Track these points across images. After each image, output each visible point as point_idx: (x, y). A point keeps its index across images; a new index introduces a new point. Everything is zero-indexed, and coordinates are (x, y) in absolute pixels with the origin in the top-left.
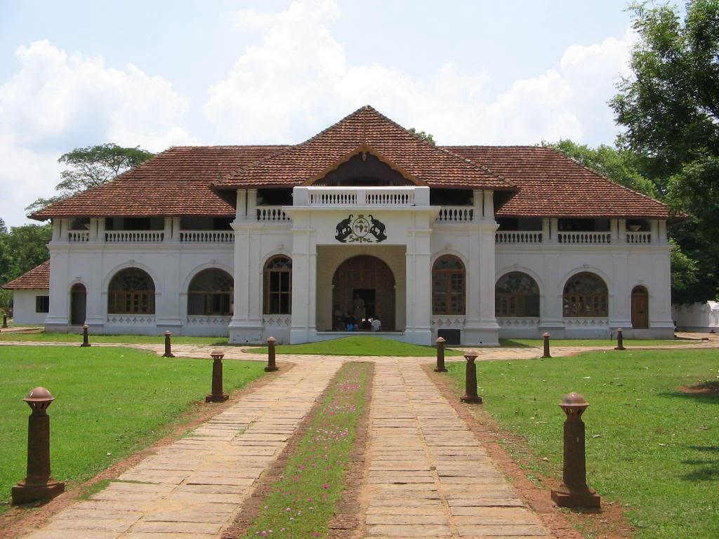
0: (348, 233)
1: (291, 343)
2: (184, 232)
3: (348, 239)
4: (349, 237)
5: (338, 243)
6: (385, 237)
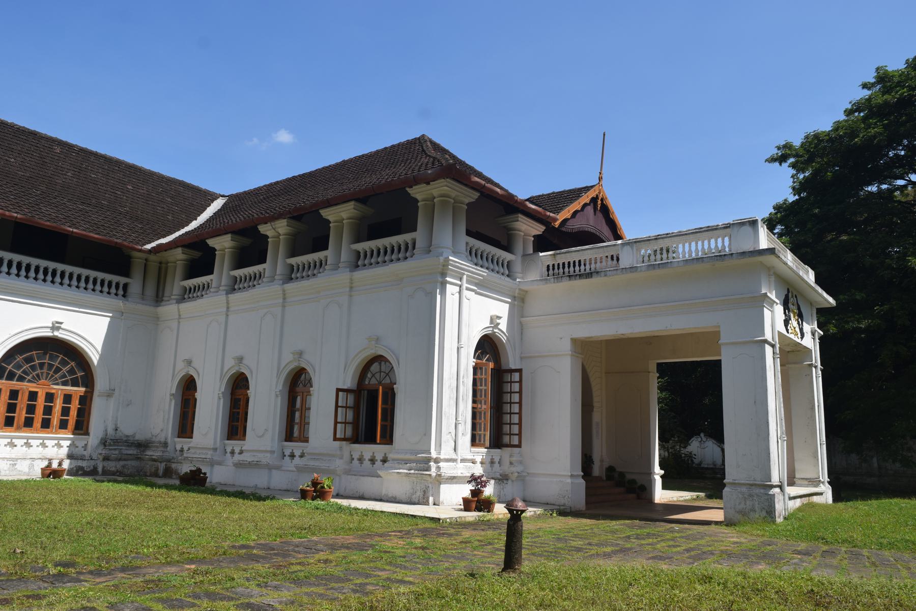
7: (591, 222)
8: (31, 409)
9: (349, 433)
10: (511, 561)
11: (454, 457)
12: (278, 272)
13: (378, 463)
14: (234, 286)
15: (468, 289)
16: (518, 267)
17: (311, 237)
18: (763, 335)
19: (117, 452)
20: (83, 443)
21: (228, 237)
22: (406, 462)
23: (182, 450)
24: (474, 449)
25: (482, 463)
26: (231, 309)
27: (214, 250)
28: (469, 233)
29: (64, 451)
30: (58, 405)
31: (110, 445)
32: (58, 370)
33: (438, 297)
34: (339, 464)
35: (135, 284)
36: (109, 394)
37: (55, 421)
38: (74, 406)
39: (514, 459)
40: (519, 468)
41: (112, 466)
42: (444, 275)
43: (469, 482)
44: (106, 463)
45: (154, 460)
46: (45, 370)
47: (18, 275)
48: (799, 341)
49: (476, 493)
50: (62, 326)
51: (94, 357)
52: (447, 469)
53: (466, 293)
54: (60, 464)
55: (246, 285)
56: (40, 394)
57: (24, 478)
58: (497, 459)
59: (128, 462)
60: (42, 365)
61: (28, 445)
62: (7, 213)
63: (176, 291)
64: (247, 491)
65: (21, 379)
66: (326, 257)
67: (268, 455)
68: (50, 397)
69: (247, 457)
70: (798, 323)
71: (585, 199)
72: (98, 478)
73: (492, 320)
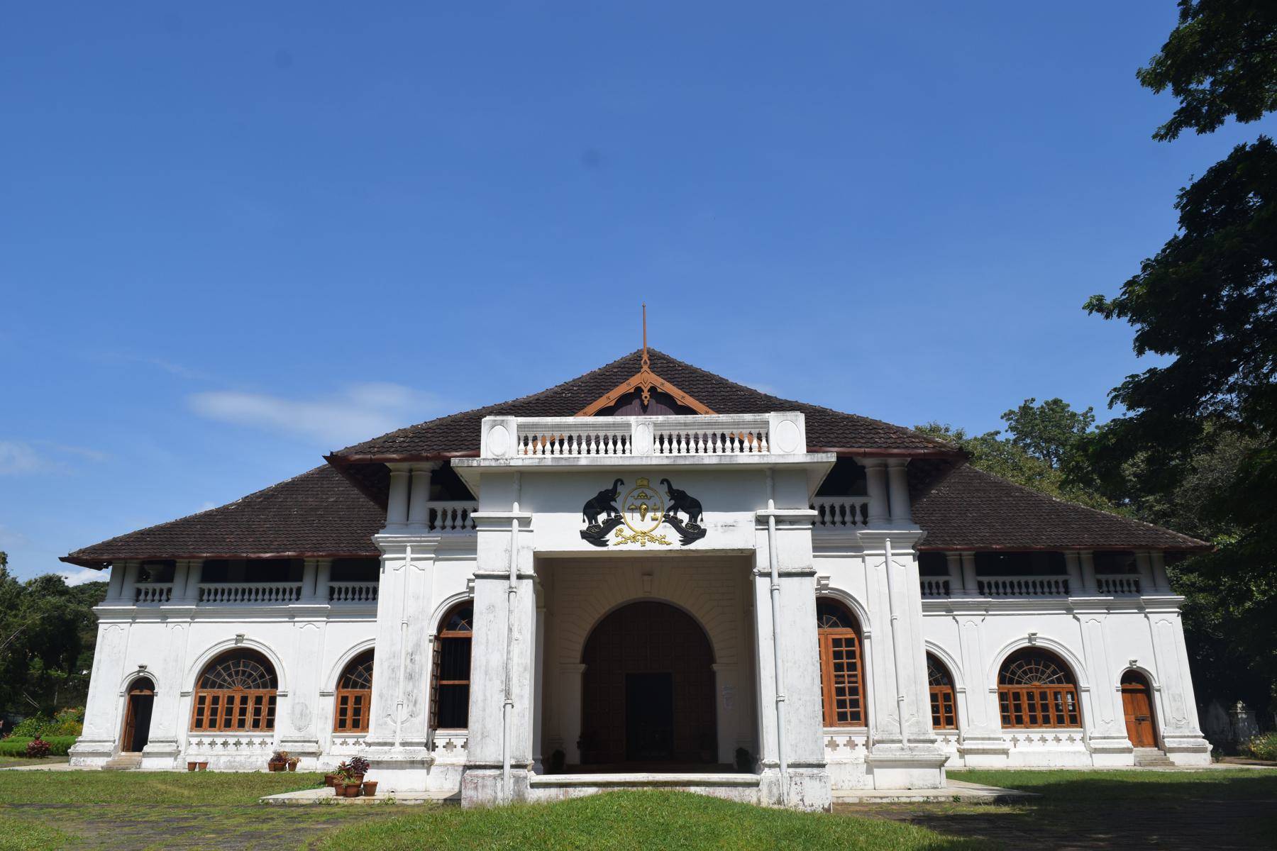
0: (610, 525)
1: (801, 418)
2: (336, 585)
3: (611, 537)
4: (614, 531)
5: (587, 546)
6: (702, 533)
32: (1043, 673)
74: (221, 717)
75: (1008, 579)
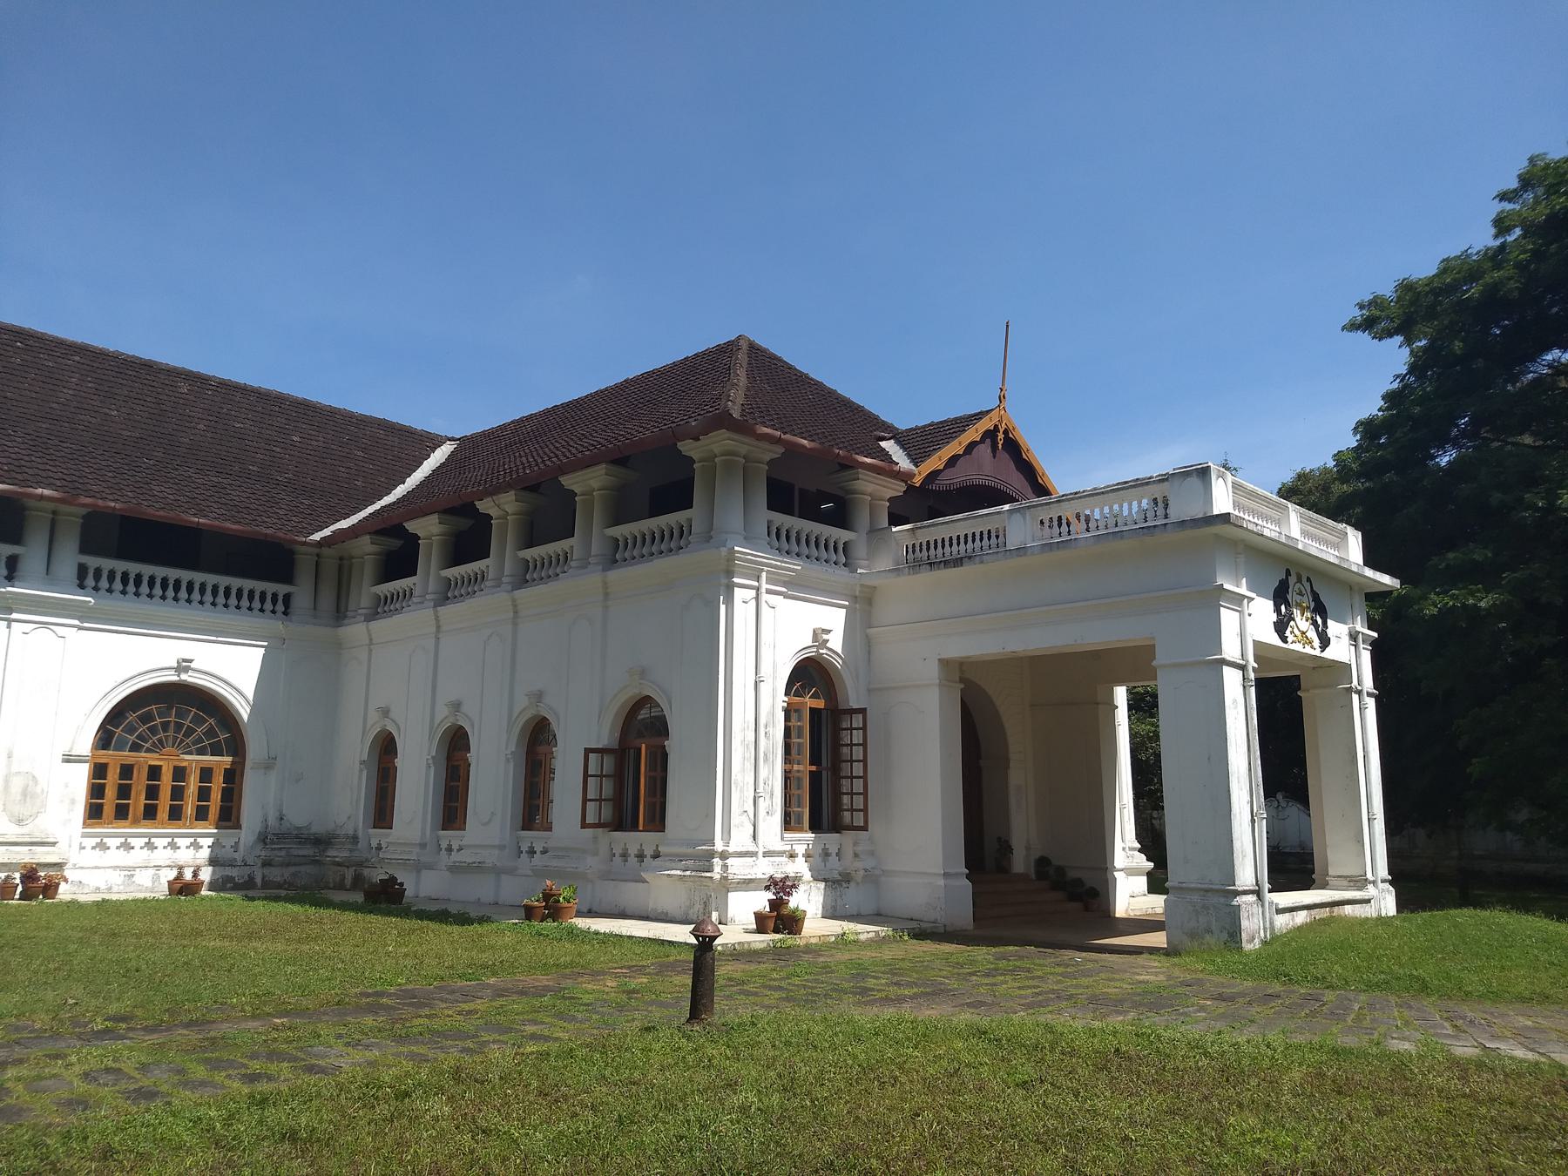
7: (988, 469)
8: (152, 792)
9: (607, 812)
10: (699, 1003)
11: (752, 848)
12: (594, 550)
13: (647, 860)
14: (525, 576)
15: (769, 592)
16: (860, 550)
17: (550, 518)
18: (1220, 651)
19: (283, 853)
20: (232, 841)
21: (434, 518)
22: (681, 858)
23: (379, 848)
24: (788, 835)
25: (807, 856)
26: (444, 628)
27: (417, 537)
28: (772, 506)
29: (205, 853)
30: (192, 785)
31: (272, 843)
32: (190, 732)
33: (723, 608)
34: (592, 864)
35: (302, 594)
36: (268, 765)
37: (189, 809)
38: (217, 785)
39: (859, 849)
40: (869, 863)
41: (276, 874)
42: (730, 574)
43: (767, 888)
44: (267, 871)
45: (339, 864)
46: (171, 733)
47: (124, 592)
48: (1317, 652)
49: (776, 905)
50: (193, 665)
51: (244, 712)
52: (739, 868)
53: (765, 597)
54: (195, 874)
55: (635, 553)
56: (164, 769)
57: (141, 896)
58: (833, 850)
59: (298, 869)
60: (165, 726)
61: (150, 846)
62: (100, 502)
63: (365, 601)
64: (453, 909)
65: (135, 748)
66: (690, 521)
67: (497, 852)
68: (180, 773)
69: (466, 857)
70: (1315, 623)
71: (973, 434)
72: (251, 893)
73: (816, 634)
74: (138, 801)
75: (248, 584)
